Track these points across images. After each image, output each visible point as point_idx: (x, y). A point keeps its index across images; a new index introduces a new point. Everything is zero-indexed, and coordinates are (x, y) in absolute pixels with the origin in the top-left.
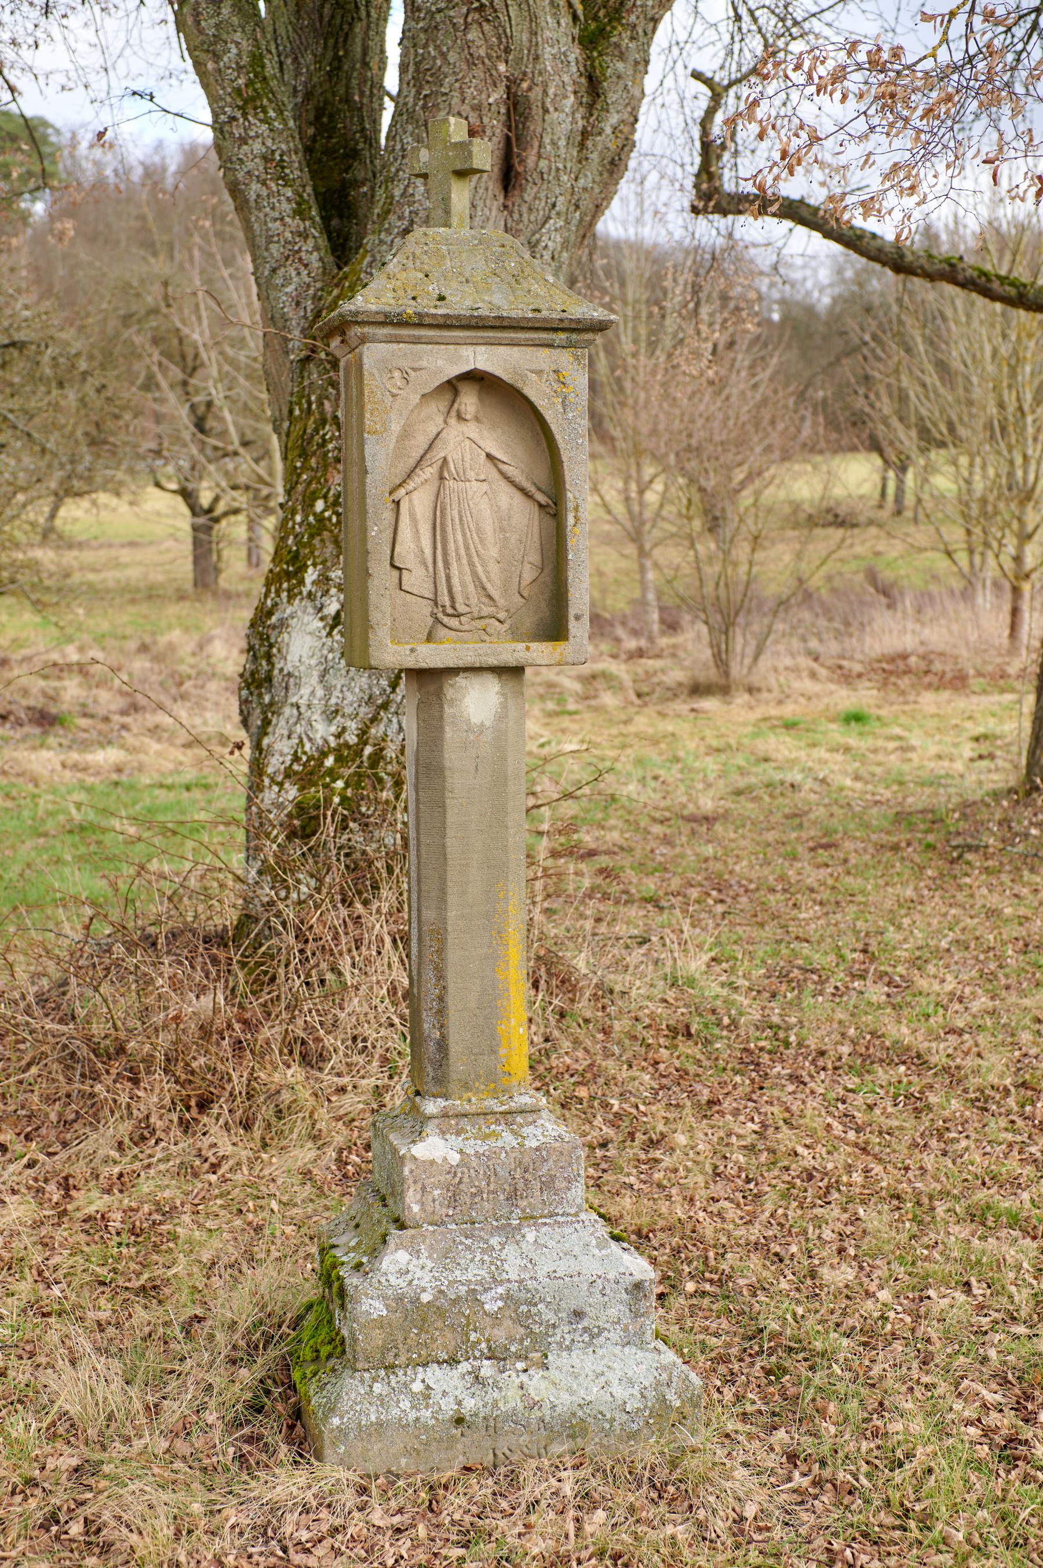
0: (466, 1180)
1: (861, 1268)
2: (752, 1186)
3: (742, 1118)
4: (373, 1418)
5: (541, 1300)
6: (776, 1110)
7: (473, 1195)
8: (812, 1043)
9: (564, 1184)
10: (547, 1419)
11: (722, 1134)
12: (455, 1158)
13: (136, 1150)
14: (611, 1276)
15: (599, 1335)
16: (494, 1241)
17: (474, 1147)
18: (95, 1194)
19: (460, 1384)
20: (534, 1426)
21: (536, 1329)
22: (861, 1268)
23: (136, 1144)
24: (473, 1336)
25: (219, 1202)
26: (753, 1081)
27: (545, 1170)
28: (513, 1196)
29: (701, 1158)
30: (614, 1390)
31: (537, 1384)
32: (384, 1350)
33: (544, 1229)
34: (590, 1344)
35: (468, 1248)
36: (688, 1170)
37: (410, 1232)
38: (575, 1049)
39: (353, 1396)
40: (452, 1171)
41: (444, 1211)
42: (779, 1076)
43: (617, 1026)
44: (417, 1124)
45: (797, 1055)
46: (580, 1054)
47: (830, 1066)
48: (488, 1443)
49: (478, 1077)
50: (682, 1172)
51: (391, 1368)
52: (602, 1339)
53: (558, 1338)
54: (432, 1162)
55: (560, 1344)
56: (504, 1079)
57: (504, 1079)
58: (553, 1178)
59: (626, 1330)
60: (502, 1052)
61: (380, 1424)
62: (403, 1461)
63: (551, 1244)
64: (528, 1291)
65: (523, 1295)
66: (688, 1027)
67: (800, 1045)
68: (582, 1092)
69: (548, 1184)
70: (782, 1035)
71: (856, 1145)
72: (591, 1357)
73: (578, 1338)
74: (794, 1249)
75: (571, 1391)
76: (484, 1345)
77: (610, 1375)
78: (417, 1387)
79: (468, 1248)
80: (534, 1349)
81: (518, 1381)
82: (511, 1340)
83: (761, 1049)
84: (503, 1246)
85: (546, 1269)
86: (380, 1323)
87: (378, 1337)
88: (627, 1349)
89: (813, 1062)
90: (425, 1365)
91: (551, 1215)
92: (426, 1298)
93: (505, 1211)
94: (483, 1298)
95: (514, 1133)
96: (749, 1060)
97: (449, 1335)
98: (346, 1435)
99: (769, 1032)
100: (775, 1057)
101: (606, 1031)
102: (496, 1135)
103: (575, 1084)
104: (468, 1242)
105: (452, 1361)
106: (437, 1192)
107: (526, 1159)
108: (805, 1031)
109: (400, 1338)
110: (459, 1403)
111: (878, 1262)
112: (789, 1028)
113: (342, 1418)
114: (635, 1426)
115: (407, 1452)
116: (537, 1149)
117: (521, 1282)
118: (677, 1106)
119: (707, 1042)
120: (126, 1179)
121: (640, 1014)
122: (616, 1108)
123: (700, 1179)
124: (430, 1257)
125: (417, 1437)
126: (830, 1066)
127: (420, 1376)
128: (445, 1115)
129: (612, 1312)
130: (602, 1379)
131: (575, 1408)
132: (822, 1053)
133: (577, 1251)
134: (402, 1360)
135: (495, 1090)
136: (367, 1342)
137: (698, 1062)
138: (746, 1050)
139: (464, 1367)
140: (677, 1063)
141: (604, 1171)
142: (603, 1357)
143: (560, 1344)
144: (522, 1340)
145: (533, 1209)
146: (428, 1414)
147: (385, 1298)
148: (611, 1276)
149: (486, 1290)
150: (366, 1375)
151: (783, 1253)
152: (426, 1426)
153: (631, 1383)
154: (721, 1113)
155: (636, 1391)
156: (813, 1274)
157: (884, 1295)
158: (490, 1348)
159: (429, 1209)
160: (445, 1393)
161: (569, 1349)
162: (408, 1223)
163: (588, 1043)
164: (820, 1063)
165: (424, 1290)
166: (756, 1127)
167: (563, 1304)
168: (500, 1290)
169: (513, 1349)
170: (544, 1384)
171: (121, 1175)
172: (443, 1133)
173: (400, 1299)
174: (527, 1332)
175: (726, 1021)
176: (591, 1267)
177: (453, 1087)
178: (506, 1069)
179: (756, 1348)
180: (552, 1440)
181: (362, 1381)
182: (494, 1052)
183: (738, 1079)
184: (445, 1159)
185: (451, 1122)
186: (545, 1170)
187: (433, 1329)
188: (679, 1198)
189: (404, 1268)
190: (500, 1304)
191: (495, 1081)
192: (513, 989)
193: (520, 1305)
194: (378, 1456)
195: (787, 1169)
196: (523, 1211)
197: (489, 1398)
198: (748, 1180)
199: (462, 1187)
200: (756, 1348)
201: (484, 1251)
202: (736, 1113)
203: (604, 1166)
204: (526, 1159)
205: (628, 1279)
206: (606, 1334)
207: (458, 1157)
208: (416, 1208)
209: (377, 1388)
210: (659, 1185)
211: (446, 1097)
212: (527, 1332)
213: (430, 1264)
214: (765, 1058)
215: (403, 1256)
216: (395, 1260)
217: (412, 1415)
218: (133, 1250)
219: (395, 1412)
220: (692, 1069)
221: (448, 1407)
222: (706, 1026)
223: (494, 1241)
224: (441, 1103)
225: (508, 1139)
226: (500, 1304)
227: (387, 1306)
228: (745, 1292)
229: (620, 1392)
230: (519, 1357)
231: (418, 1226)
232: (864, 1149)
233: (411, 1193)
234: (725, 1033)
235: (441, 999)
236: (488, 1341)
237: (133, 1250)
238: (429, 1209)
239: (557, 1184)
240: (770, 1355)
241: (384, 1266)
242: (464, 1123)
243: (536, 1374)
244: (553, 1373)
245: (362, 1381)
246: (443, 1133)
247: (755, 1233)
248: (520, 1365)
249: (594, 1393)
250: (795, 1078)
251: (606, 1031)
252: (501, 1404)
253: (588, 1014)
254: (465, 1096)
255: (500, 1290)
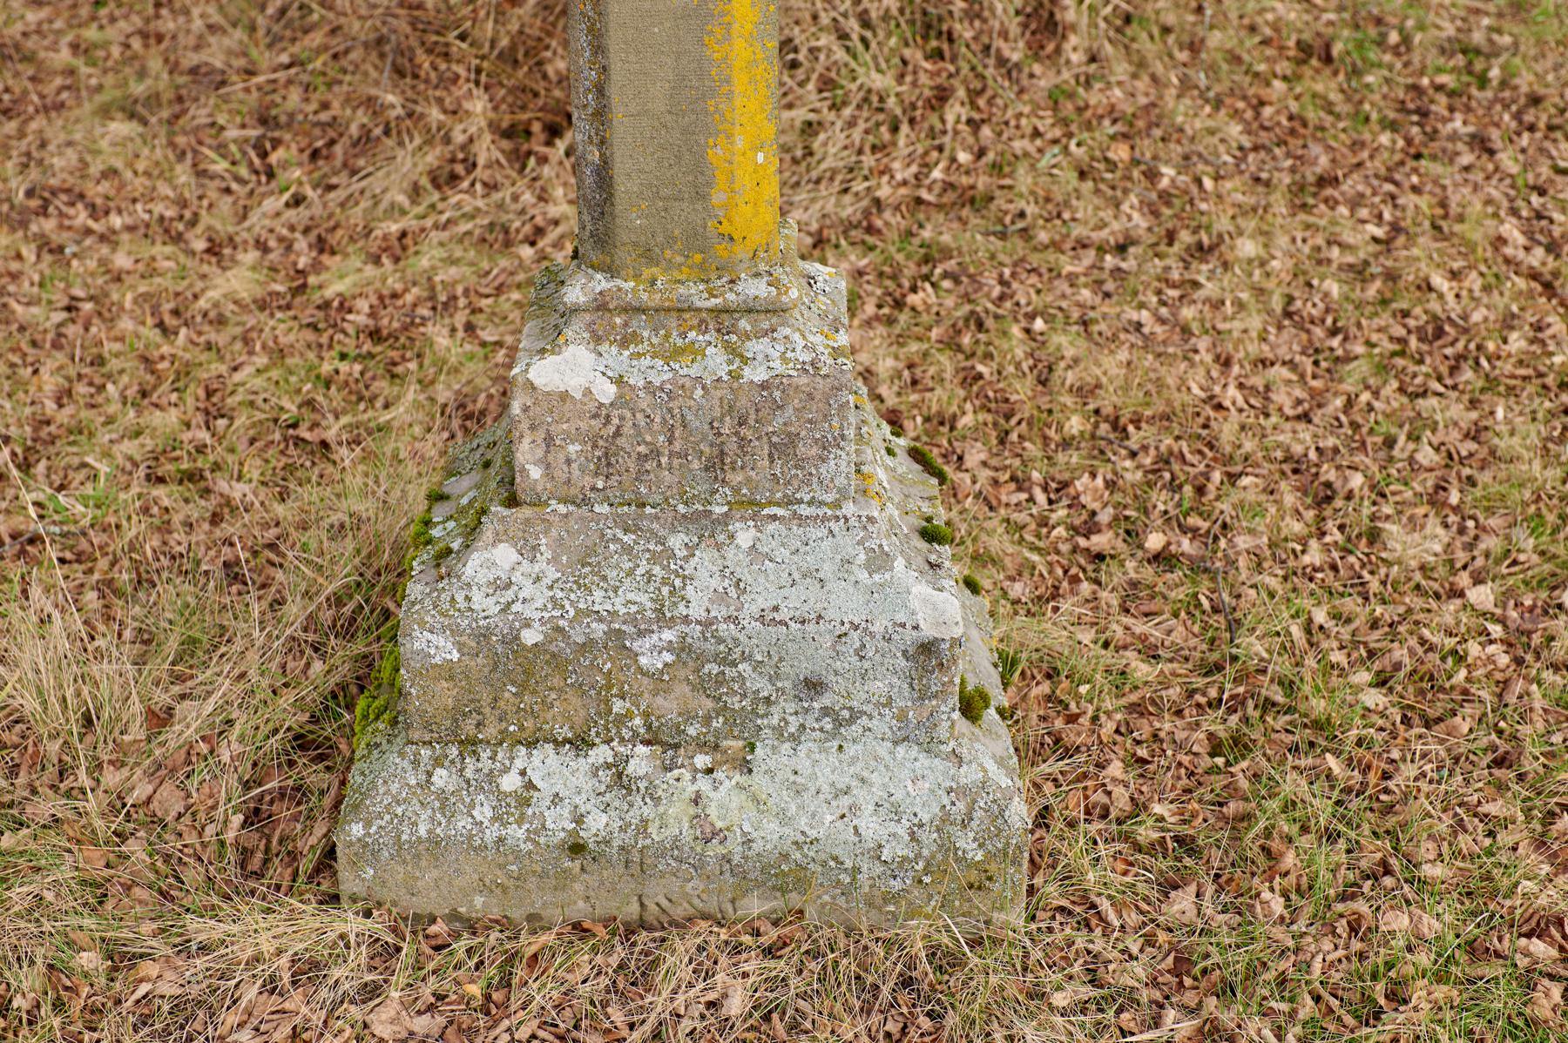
0: (628, 429)
1: (1462, 531)
2: (1335, 342)
3: (1364, 213)
4: (422, 831)
5: (745, 658)
6: (1423, 202)
7: (642, 458)
8: (1524, 82)
9: (814, 451)
10: (736, 859)
11: (1320, 240)
12: (606, 392)
13: (436, 196)
14: (877, 628)
15: (852, 721)
16: (677, 541)
17: (648, 371)
18: (356, 262)
19: (588, 784)
20: (712, 866)
21: (734, 702)
22: (1462, 531)
23: (438, 187)
24: (618, 706)
25: (516, 296)
26: (1409, 141)
27: (778, 423)
28: (717, 465)
29: (1270, 284)
30: (861, 823)
31: (725, 798)
32: (457, 715)
33: (772, 527)
34: (834, 734)
35: (627, 550)
36: (1240, 305)
37: (525, 512)
38: (1135, 76)
39: (395, 787)
40: (601, 413)
41: (588, 481)
42: (1453, 137)
43: (1215, 39)
44: (552, 321)
45: (1496, 100)
46: (1142, 84)
47: (1542, 125)
48: (628, 886)
49: (671, 240)
50: (1229, 308)
51: (470, 745)
52: (856, 729)
53: (775, 721)
54: (564, 396)
55: (779, 731)
56: (721, 249)
57: (721, 249)
58: (793, 439)
59: (902, 717)
60: (717, 198)
61: (434, 842)
62: (479, 901)
63: (782, 554)
64: (720, 641)
65: (710, 646)
66: (1328, 47)
67: (1504, 84)
68: (1121, 153)
69: (784, 448)
70: (1478, 66)
71: (1534, 276)
72: (833, 757)
73: (810, 722)
74: (1357, 481)
75: (783, 818)
76: (638, 721)
77: (859, 793)
78: (510, 782)
79: (627, 550)
80: (731, 739)
81: (691, 790)
82: (690, 717)
83: (1439, 88)
84: (691, 550)
85: (761, 602)
86: (448, 672)
87: (446, 695)
88: (901, 750)
89: (1517, 117)
90: (531, 744)
91: (788, 502)
92: (530, 637)
93: (702, 488)
94: (636, 646)
95: (733, 352)
96: (1415, 108)
97: (576, 701)
98: (375, 854)
99: (1460, 60)
100: (1458, 102)
101: (1194, 47)
102: (696, 352)
103: (1113, 138)
104: (628, 539)
105: (580, 743)
106: (573, 448)
107: (743, 403)
108: (1517, 61)
109: (486, 698)
110: (579, 820)
111: (1493, 522)
112: (1495, 52)
113: (368, 824)
114: (896, 885)
115: (484, 887)
116: (764, 386)
117: (707, 624)
118: (1267, 184)
119: (1356, 72)
120: (408, 241)
121: (1259, 20)
122: (1164, 183)
123: (1255, 322)
124: (554, 560)
125: (502, 867)
126: (1542, 125)
127: (519, 764)
128: (601, 305)
129: (879, 687)
130: (845, 801)
131: (787, 846)
132: (1535, 100)
133: (827, 570)
134: (491, 731)
135: (702, 266)
136: (426, 697)
137: (1329, 107)
138: (1415, 88)
139: (601, 754)
140: (1294, 106)
141: (1107, 295)
142: (854, 760)
143: (779, 731)
144: (707, 720)
145: (754, 489)
146: (520, 833)
147: (455, 631)
148: (877, 628)
149: (641, 634)
150: (425, 753)
151: (1338, 485)
152: (517, 855)
153: (897, 813)
154: (1332, 203)
155: (902, 831)
156: (1374, 536)
157: (1483, 596)
158: (649, 727)
159: (561, 475)
160: (556, 799)
161: (795, 739)
162: (522, 496)
163: (1159, 68)
164: (1528, 118)
165: (527, 624)
166: (1380, 232)
167: (785, 668)
168: (668, 635)
169: (692, 731)
170: (738, 799)
171: (404, 234)
172: (598, 339)
173: (484, 635)
174: (723, 708)
175: (1394, 37)
176: (845, 603)
177: (624, 255)
178: (726, 228)
179: (1213, 693)
180: (745, 893)
181: (416, 763)
182: (701, 196)
183: (1385, 139)
184: (588, 392)
185: (612, 322)
186: (778, 423)
187: (536, 689)
188: (1208, 358)
189: (507, 578)
190: (668, 657)
191: (706, 250)
192: (740, 81)
193: (706, 662)
194: (431, 890)
195: (1406, 314)
196: (736, 490)
197: (633, 817)
198: (1333, 332)
199: (621, 441)
200: (1213, 693)
201: (654, 558)
202: (1356, 202)
203: (1110, 286)
204: (743, 403)
205: (910, 636)
206: (864, 720)
207: (612, 389)
208: (535, 473)
209: (441, 777)
210: (1186, 331)
211: (611, 271)
212: (723, 708)
213: (552, 574)
214: (1440, 105)
215: (505, 555)
216: (492, 559)
217: (491, 834)
218: (358, 367)
219: (463, 823)
220: (1312, 115)
221: (558, 823)
222: (1360, 45)
223: (677, 541)
224: (601, 282)
225: (717, 361)
226: (668, 657)
227: (460, 647)
228: (1242, 562)
229: (871, 826)
230: (702, 746)
231: (538, 503)
232: (1548, 286)
233: (525, 445)
234: (1387, 58)
235: (600, 90)
236: (646, 715)
237: (358, 367)
238: (561, 475)
239: (801, 449)
240: (1231, 710)
241: (469, 571)
242: (639, 323)
243: (729, 779)
244: (759, 781)
245: (416, 763)
246: (598, 339)
247: (1302, 440)
248: (702, 760)
249: (823, 823)
250: (1481, 144)
251: (1194, 47)
252: (653, 829)
253: (1170, 19)
254: (647, 273)
255: (668, 635)
